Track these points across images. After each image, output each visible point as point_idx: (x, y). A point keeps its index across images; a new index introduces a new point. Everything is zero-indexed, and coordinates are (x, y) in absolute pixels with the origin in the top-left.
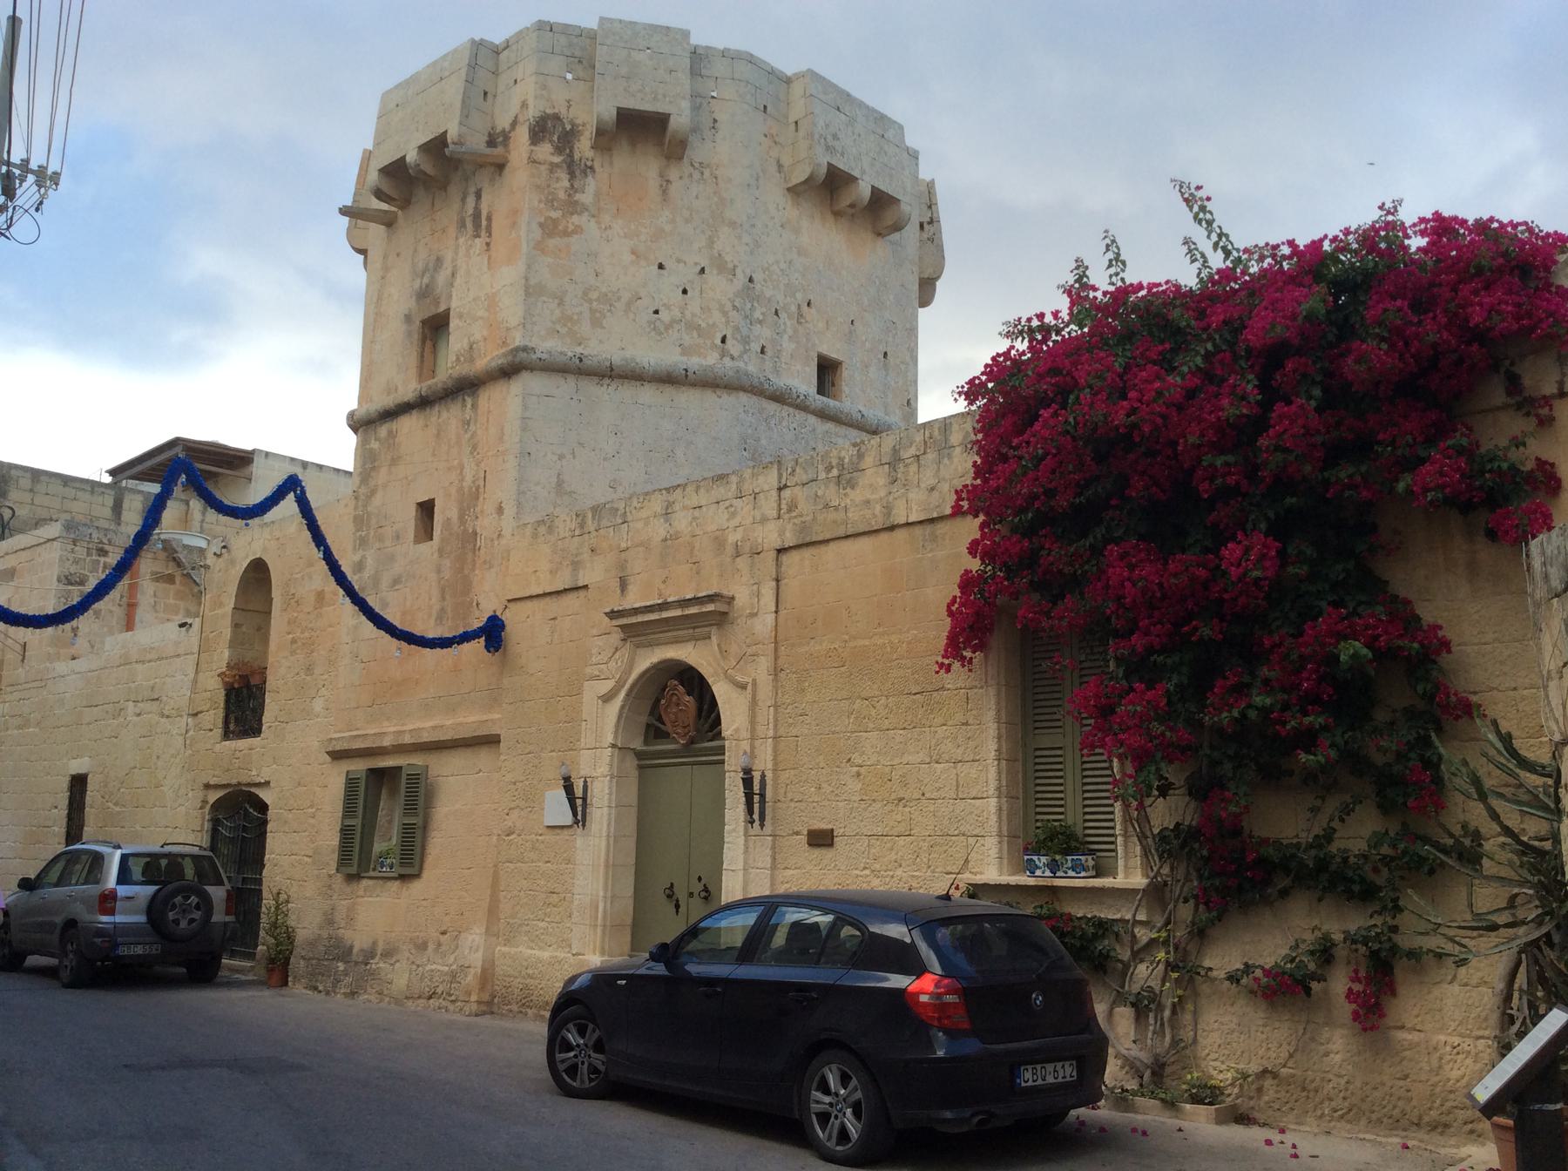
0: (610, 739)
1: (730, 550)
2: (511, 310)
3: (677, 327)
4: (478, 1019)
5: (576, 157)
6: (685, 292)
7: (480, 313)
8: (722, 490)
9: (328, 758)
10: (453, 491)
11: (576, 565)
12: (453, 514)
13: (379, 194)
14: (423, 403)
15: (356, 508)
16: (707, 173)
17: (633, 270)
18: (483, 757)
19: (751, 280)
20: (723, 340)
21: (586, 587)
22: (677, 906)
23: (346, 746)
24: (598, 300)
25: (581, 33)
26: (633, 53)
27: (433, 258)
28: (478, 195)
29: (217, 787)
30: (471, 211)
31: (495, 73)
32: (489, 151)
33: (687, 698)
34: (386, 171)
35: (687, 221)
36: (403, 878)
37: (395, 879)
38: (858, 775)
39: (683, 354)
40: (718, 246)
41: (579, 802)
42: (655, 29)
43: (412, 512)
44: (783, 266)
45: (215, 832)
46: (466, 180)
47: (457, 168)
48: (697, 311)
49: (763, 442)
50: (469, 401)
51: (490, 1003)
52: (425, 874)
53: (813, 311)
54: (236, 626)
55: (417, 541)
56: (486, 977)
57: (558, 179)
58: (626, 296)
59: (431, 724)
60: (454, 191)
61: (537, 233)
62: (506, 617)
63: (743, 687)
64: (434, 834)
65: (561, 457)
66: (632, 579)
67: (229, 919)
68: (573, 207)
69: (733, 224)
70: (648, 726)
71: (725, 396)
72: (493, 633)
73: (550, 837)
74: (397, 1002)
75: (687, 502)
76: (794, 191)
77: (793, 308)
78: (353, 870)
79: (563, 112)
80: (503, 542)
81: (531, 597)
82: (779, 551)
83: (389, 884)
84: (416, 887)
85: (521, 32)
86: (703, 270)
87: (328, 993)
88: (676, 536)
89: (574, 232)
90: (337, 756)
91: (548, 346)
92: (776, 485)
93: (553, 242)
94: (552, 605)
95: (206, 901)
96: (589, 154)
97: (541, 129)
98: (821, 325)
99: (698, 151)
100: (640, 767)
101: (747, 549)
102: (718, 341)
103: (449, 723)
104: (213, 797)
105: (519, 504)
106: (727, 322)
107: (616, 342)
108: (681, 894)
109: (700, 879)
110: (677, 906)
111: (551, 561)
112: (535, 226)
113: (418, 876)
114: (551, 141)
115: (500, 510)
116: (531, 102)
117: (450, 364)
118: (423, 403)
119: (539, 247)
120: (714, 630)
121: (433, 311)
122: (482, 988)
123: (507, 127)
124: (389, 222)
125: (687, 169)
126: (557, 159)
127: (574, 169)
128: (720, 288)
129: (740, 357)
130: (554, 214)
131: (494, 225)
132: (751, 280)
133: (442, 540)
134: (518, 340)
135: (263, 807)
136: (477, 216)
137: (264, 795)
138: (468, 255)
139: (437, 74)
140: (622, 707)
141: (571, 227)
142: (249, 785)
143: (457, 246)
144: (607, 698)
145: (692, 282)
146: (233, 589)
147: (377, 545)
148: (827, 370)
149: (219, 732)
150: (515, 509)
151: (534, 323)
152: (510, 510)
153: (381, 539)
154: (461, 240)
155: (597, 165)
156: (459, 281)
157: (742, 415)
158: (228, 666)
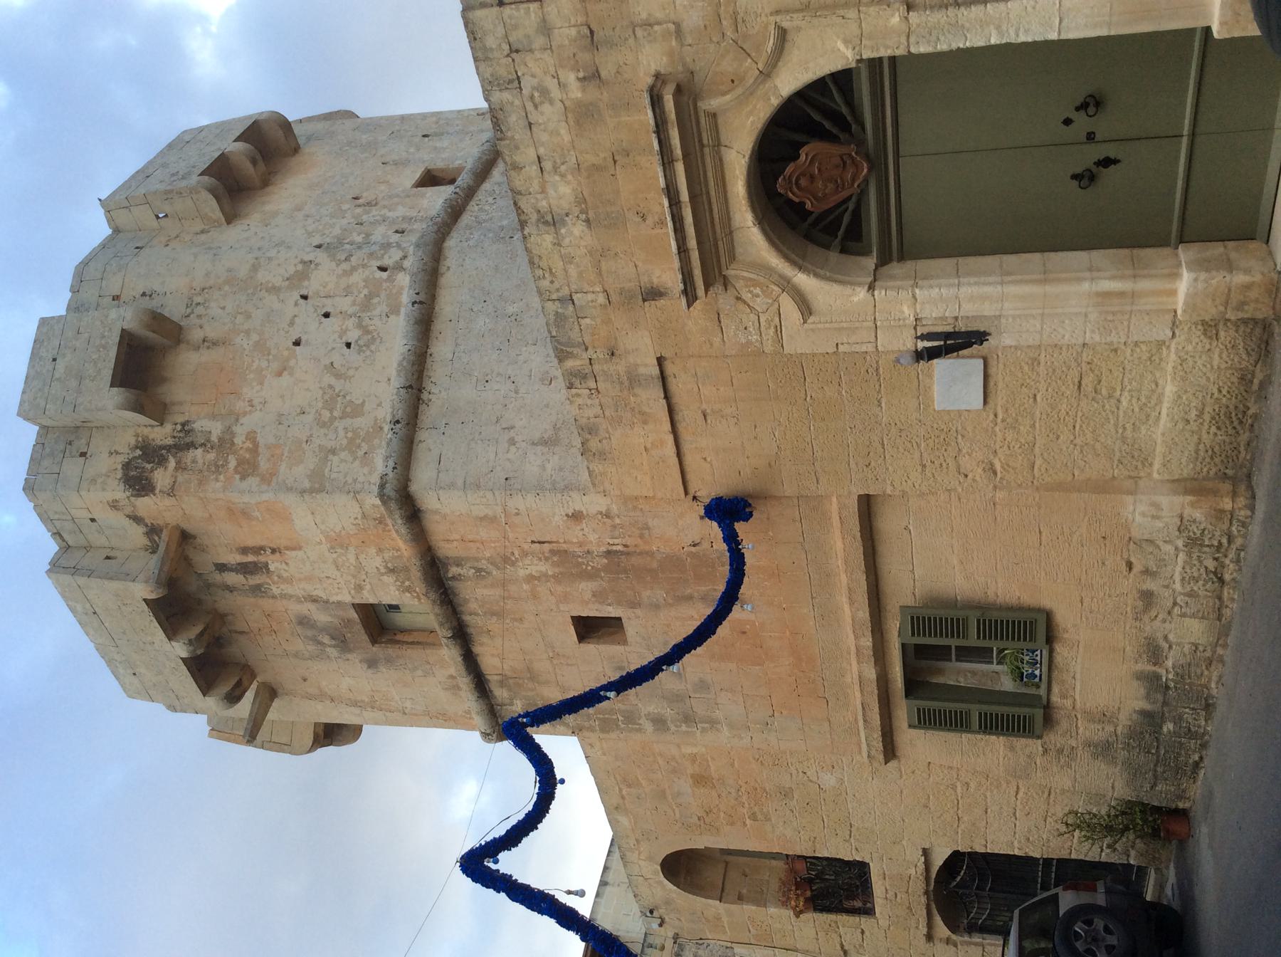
0: (861, 294)
1: (593, 94)
3: (366, 321)
4: (1260, 493)
5: (170, 441)
6: (327, 315)
7: (352, 560)
8: (513, 119)
10: (560, 589)
11: (633, 380)
12: (586, 587)
13: (233, 698)
14: (462, 636)
15: (591, 729)
17: (298, 371)
18: (889, 523)
19: (319, 247)
21: (660, 361)
22: (1107, 162)
23: (877, 734)
24: (331, 411)
25: (40, 444)
26: (57, 375)
27: (299, 629)
28: (222, 568)
29: (930, 925)
31: (88, 548)
33: (803, 157)
34: (206, 686)
35: (249, 316)
36: (1050, 640)
37: (1051, 652)
39: (397, 312)
40: (278, 281)
42: (35, 355)
43: (591, 648)
45: (984, 930)
48: (349, 299)
49: (505, 223)
50: (454, 571)
51: (1234, 480)
52: (1046, 603)
54: (740, 898)
56: (1194, 487)
57: (194, 461)
58: (328, 379)
59: (846, 608)
61: (253, 481)
62: (707, 493)
63: (783, 34)
64: (991, 597)
65: (512, 442)
66: (645, 279)
67: (1101, 887)
68: (225, 444)
69: (255, 268)
70: (843, 251)
71: (448, 263)
72: (729, 511)
73: (1000, 399)
74: (1224, 632)
75: (535, 186)
76: (230, 218)
77: (359, 210)
78: (1039, 713)
79: (122, 459)
80: (614, 509)
81: (679, 455)
83: (1058, 659)
84: (1065, 617)
85: (40, 515)
86: (305, 297)
87: (1204, 746)
88: (581, 200)
90: (890, 751)
93: (264, 464)
94: (688, 416)
95: (1075, 913)
96: (168, 428)
97: (138, 483)
98: (383, 187)
99: (174, 309)
100: (902, 258)
101: (585, 57)
102: (384, 275)
103: (844, 578)
104: (942, 930)
106: (364, 266)
107: (379, 385)
109: (1067, 122)
110: (1107, 162)
111: (632, 425)
112: (244, 485)
113: (1049, 616)
114: (152, 471)
115: (576, 517)
116: (110, 496)
117: (418, 608)
118: (462, 636)
119: (267, 479)
120: (704, 105)
121: (359, 627)
122: (1215, 493)
124: (270, 693)
126: (172, 463)
127: (185, 442)
128: (325, 276)
129: (403, 250)
130: (233, 463)
131: (250, 543)
132: (319, 247)
133: (619, 603)
135: (956, 858)
136: (245, 569)
137: (939, 860)
138: (289, 581)
139: (90, 618)
141: (248, 444)
142: (927, 878)
143: (284, 596)
144: (806, 308)
145: (316, 308)
146: (698, 902)
149: (864, 921)
150: (575, 495)
151: (355, 481)
152: (577, 502)
154: (276, 591)
155: (181, 419)
156: (320, 593)
157: (471, 243)
158: (785, 904)
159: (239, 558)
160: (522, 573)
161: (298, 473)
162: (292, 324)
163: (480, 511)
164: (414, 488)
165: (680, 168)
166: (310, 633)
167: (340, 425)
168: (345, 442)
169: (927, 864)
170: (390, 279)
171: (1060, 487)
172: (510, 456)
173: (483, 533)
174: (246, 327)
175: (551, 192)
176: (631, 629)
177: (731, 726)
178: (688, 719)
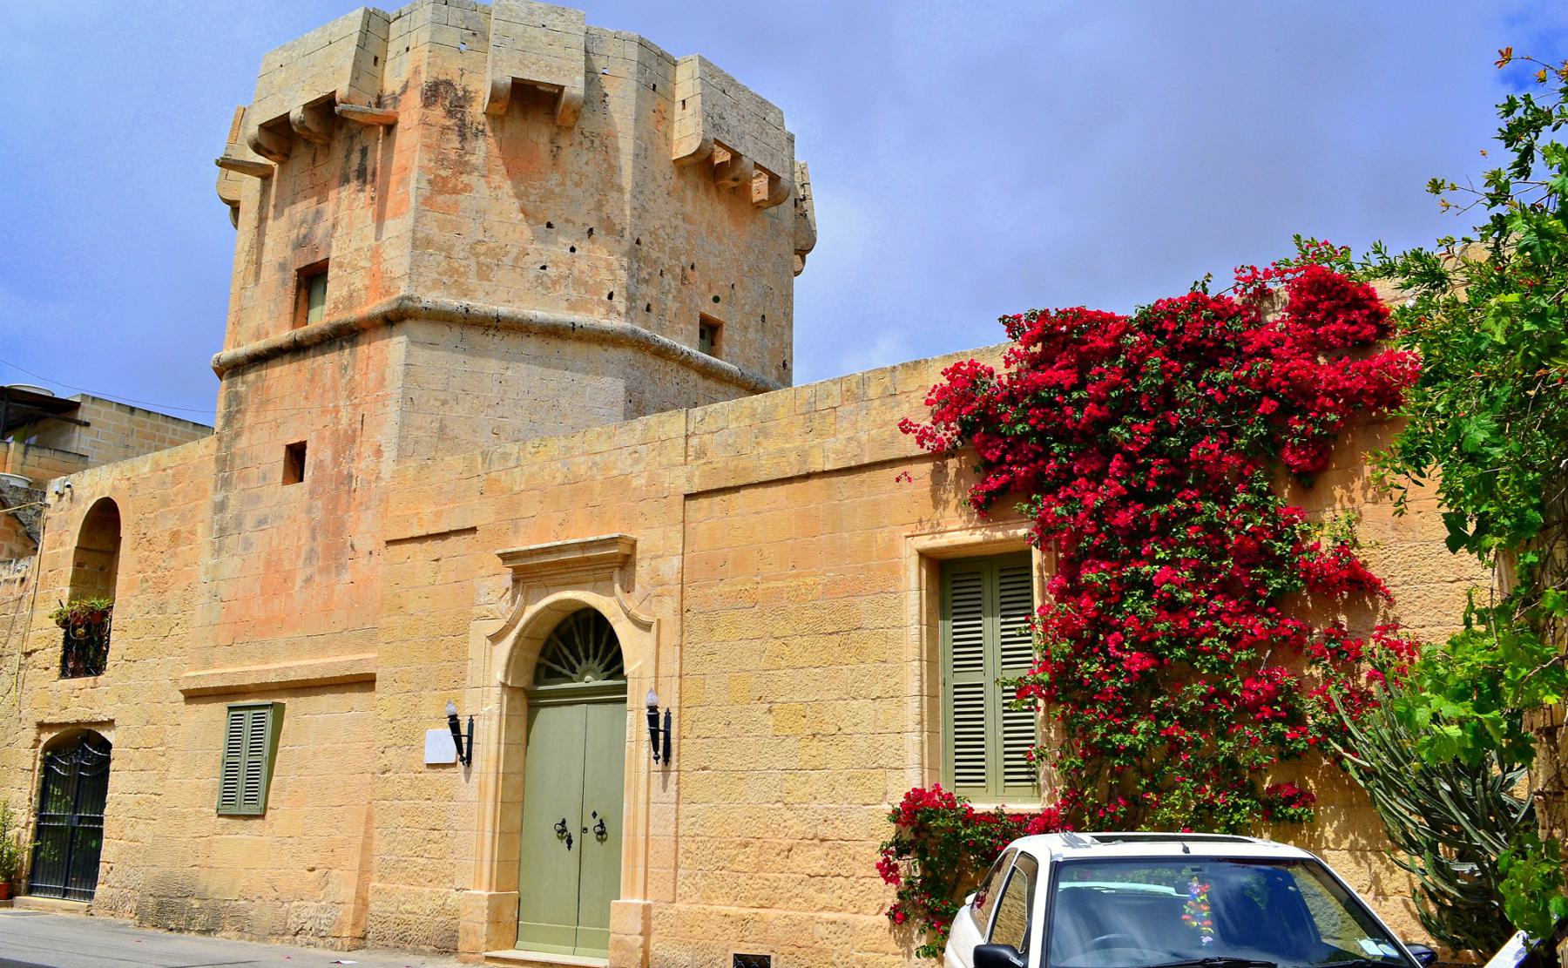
2: (397, 259)
5: (468, 120)
7: (363, 263)
9: (182, 697)
10: (327, 434)
12: (327, 455)
14: (296, 349)
15: (219, 450)
16: (597, 143)
18: (355, 698)
20: (610, 296)
21: (474, 530)
28: (364, 152)
30: (356, 167)
31: (386, 40)
32: (377, 111)
35: (577, 185)
38: (770, 711)
40: (607, 209)
41: (464, 740)
43: (281, 455)
44: (668, 230)
46: (352, 138)
47: (340, 128)
49: (648, 395)
53: (697, 273)
54: (78, 565)
55: (286, 481)
58: (515, 251)
60: (339, 149)
61: (427, 190)
68: (462, 166)
70: (539, 666)
71: (611, 350)
73: (431, 775)
77: (678, 270)
79: (456, 81)
82: (688, 497)
89: (464, 190)
91: (433, 297)
92: (683, 432)
93: (441, 199)
94: (436, 547)
97: (435, 92)
98: (703, 287)
102: (605, 298)
104: (46, 737)
105: (400, 448)
108: (573, 829)
109: (594, 815)
110: (570, 842)
112: (424, 184)
115: (378, 453)
116: (424, 68)
117: (321, 318)
118: (296, 349)
119: (427, 201)
121: (311, 261)
123: (398, 91)
125: (578, 138)
130: (443, 173)
132: (638, 242)
133: (314, 481)
134: (403, 290)
135: (106, 746)
137: (104, 734)
138: (350, 208)
140: (514, 646)
142: (90, 723)
144: (496, 638)
147: (242, 486)
148: (710, 331)
153: (245, 479)
159: (370, 169)
160: (342, 403)
161: (431, 228)
162: (567, 221)
163: (388, 372)
164: (409, 324)
165: (578, 555)
166: (310, 217)
167: (472, 262)
168: (456, 265)
169: (101, 724)
170: (600, 302)
171: (369, 818)
172: (432, 402)
173: (372, 375)
174: (568, 182)
175: (582, 459)
176: (294, 488)
177: (216, 567)
178: (223, 532)
